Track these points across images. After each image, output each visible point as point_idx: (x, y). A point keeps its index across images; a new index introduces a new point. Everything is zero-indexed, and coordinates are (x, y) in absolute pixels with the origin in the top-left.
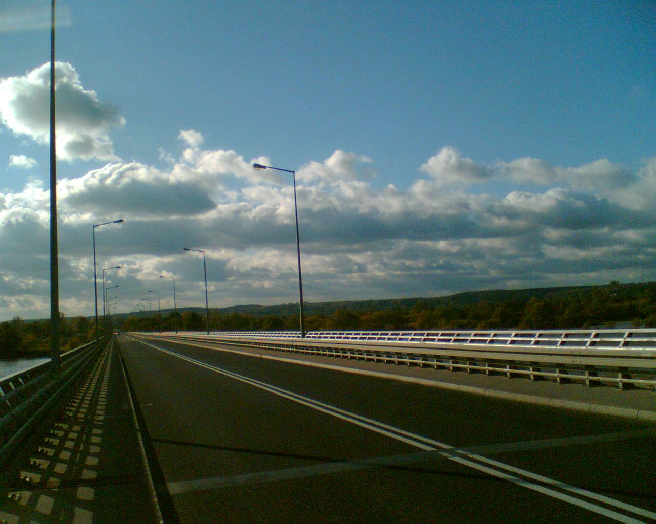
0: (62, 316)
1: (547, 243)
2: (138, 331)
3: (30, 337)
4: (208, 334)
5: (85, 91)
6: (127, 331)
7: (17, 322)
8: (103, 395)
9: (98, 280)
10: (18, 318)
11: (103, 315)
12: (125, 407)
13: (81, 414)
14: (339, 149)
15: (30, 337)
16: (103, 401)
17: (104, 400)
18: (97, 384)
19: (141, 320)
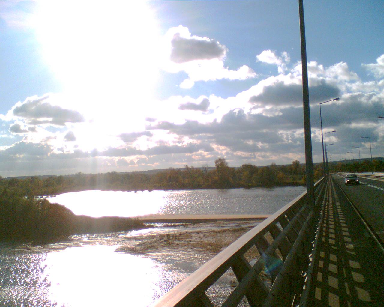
0: (299, 163)
1: (10, 122)
2: (345, 172)
3: (281, 174)
4: (373, 173)
5: (220, 46)
6: (338, 172)
7: (274, 166)
8: (342, 220)
9: (317, 133)
10: (274, 164)
11: (323, 162)
12: (369, 237)
13: (332, 227)
14: (348, 64)
15: (281, 174)
16: (332, 211)
17: (330, 210)
18: (333, 211)
19: (347, 165)
